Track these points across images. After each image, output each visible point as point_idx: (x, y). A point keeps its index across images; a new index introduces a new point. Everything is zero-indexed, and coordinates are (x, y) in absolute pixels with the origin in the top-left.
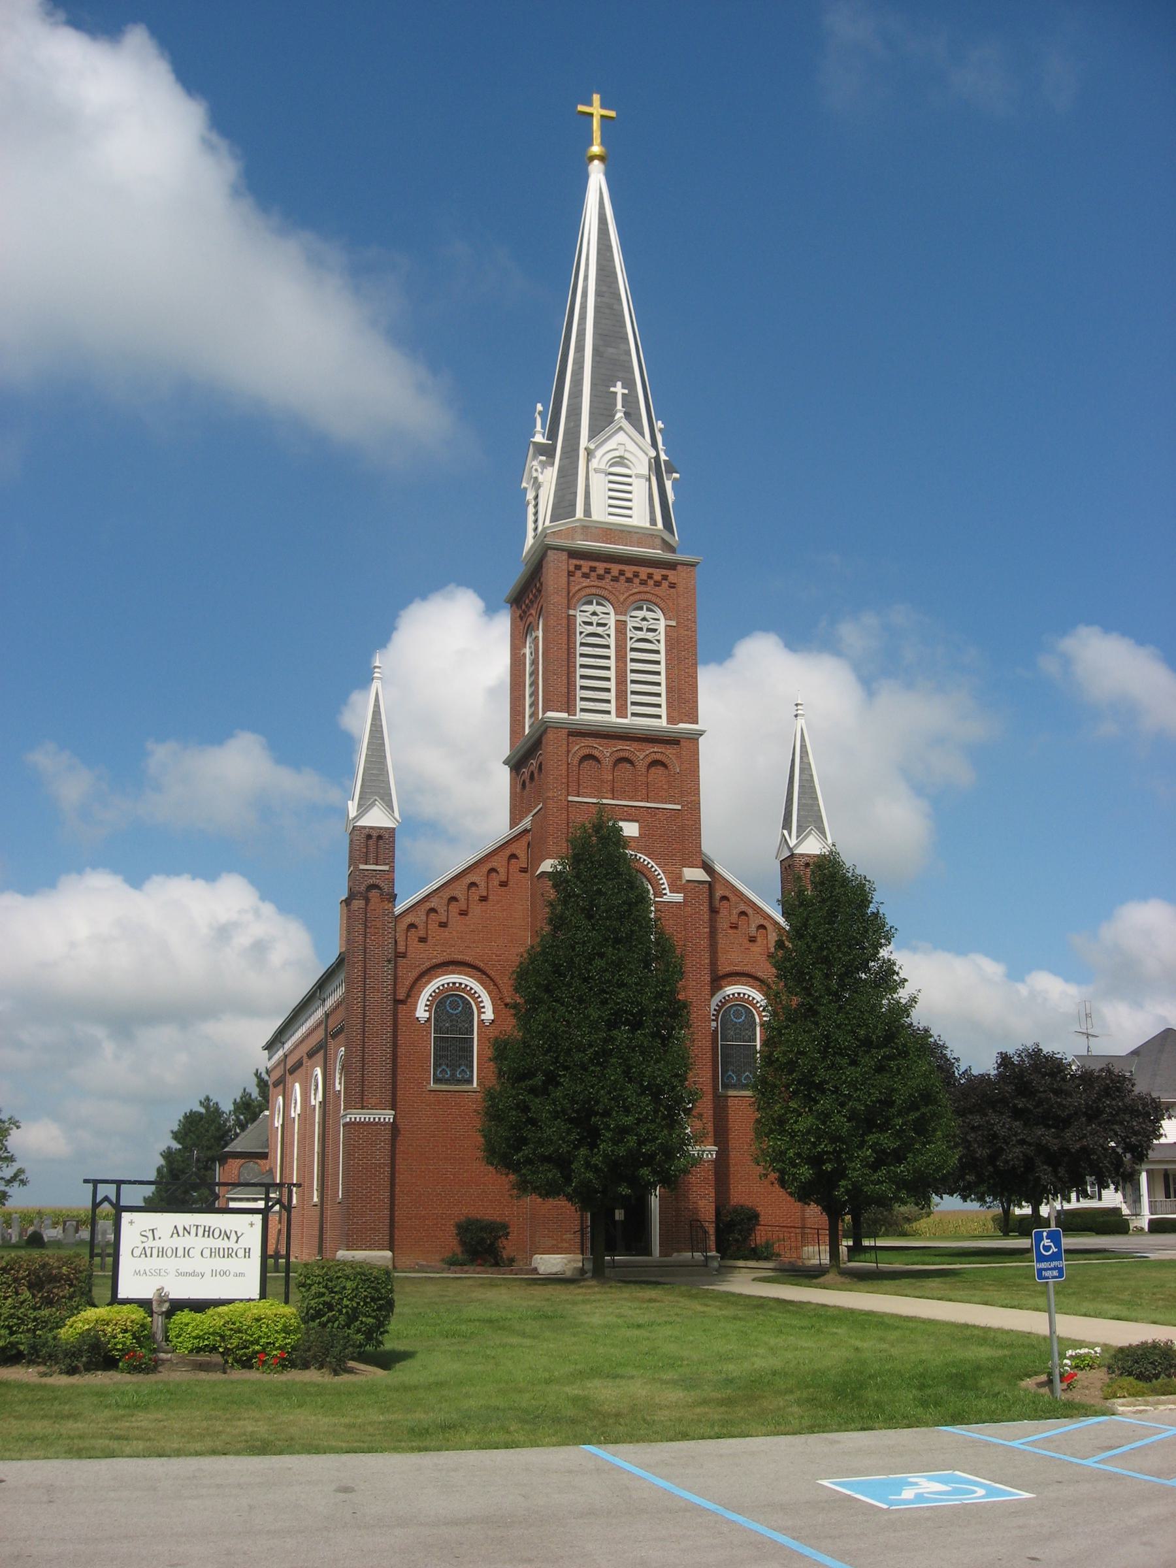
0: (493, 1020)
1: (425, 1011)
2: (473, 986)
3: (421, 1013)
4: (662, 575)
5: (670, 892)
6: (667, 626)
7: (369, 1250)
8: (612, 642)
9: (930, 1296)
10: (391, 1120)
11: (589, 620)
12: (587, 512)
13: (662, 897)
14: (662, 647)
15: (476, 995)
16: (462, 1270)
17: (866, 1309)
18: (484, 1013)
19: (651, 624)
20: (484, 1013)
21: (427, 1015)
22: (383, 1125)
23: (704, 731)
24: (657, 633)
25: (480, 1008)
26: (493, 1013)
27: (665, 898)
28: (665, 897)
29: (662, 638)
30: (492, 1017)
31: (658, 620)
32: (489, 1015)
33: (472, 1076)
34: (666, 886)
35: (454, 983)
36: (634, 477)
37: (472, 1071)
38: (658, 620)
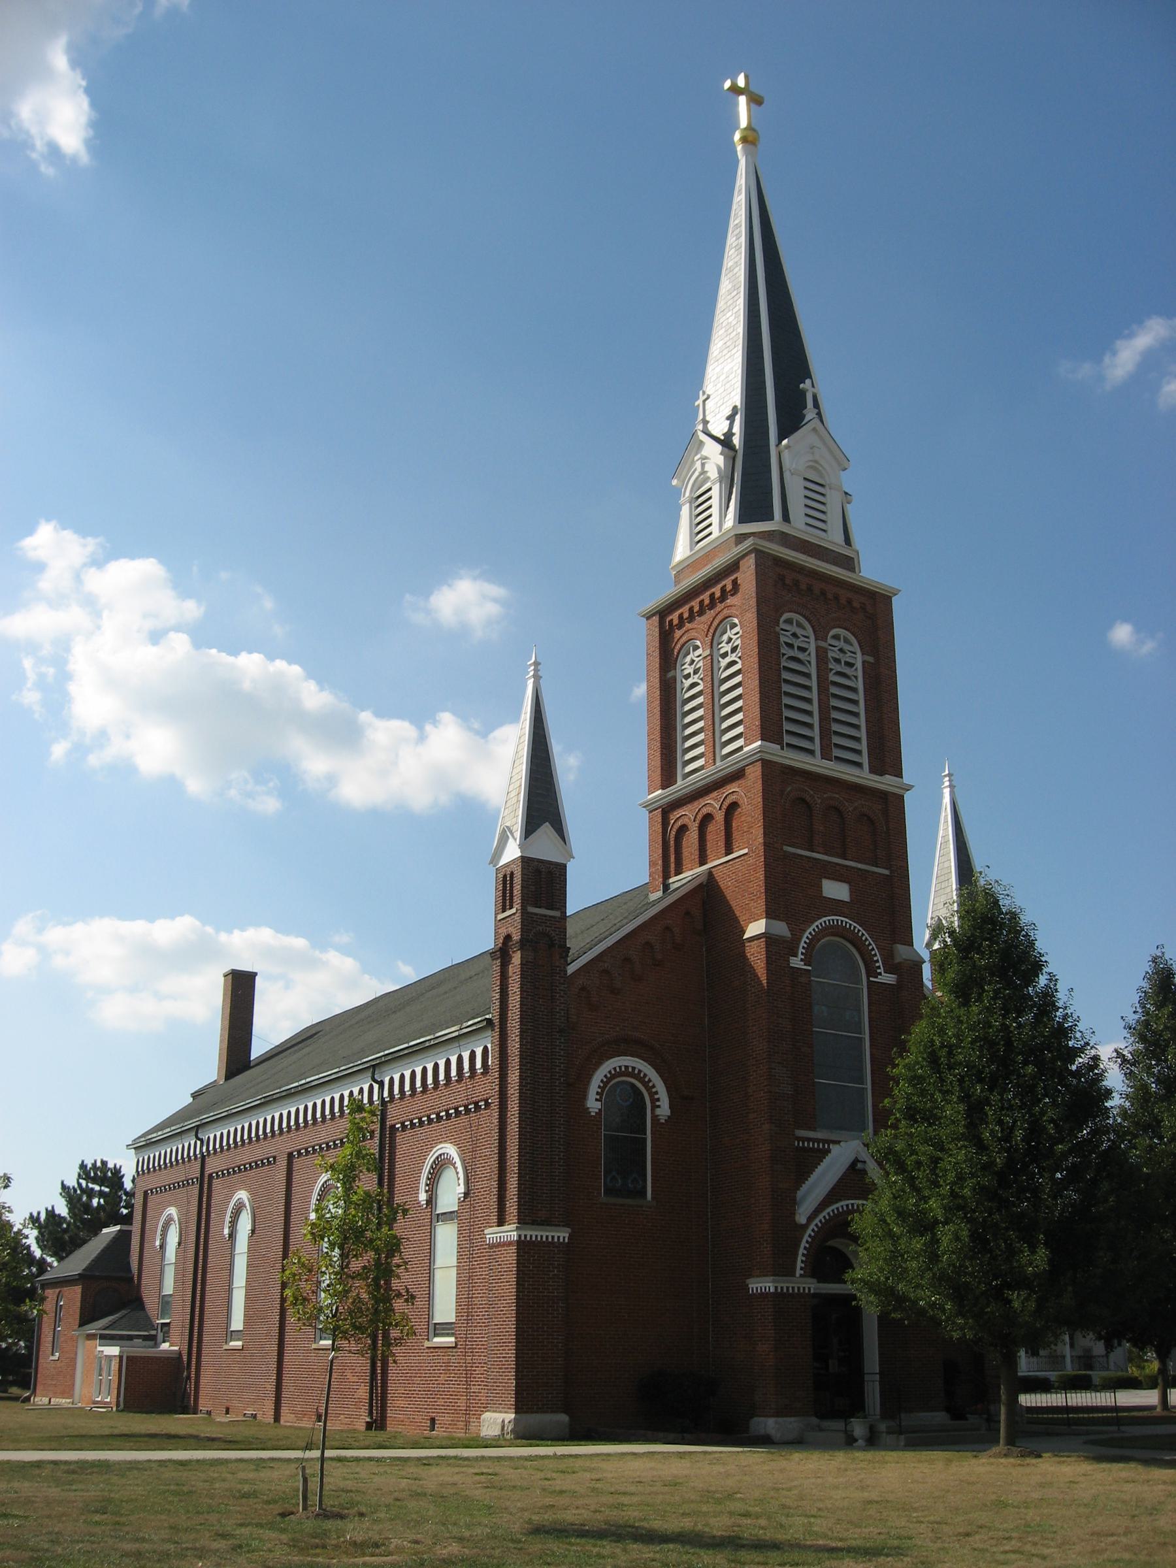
0: (669, 1117)
1: (597, 1100)
2: (647, 1073)
3: (593, 1104)
4: (860, 603)
5: (885, 972)
6: (864, 662)
7: (552, 1412)
8: (813, 671)
9: (40, 1447)
10: (566, 1240)
11: (790, 642)
12: (786, 517)
13: (877, 977)
14: (860, 685)
15: (651, 1084)
16: (683, 1438)
17: (5, 1459)
18: (659, 1106)
19: (847, 658)
20: (659, 1106)
21: (598, 1105)
22: (557, 1247)
23: (913, 786)
24: (855, 667)
25: (654, 1101)
26: (670, 1108)
27: (880, 979)
28: (879, 977)
29: (860, 674)
30: (668, 1113)
31: (854, 653)
32: (664, 1110)
33: (645, 1187)
34: (880, 964)
35: (627, 1067)
36: (827, 487)
37: (645, 1181)
38: (854, 653)
